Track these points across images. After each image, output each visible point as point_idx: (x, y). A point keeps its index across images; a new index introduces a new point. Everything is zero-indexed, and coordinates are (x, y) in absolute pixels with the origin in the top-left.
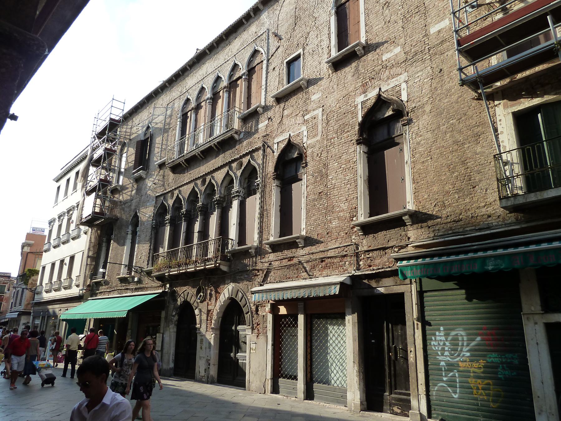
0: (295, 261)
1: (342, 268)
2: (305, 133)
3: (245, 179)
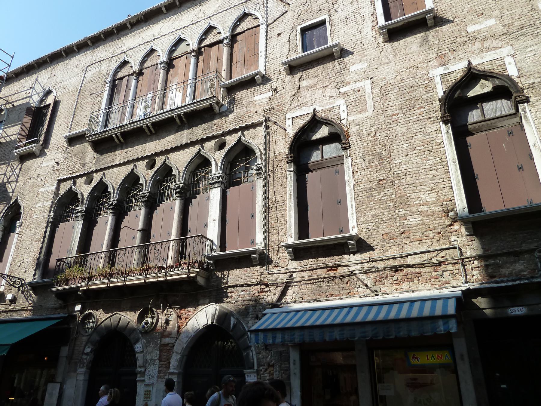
0: (341, 271)
1: (438, 280)
2: (343, 107)
3: (229, 162)
